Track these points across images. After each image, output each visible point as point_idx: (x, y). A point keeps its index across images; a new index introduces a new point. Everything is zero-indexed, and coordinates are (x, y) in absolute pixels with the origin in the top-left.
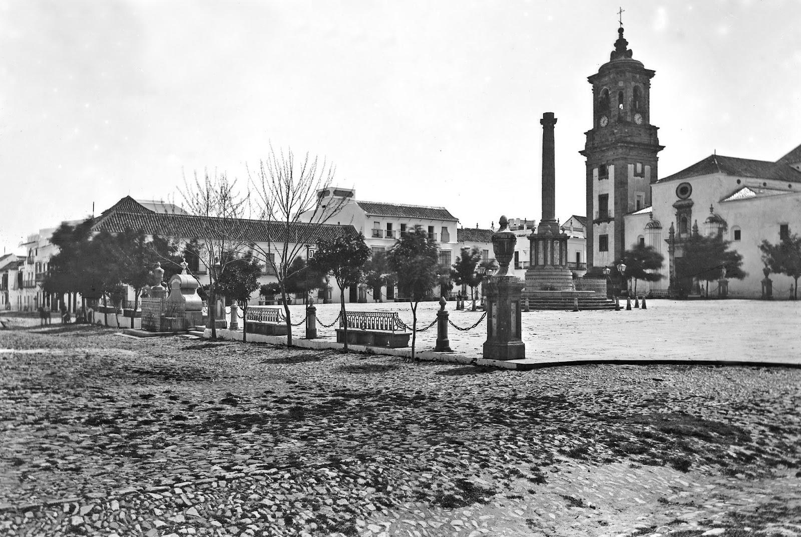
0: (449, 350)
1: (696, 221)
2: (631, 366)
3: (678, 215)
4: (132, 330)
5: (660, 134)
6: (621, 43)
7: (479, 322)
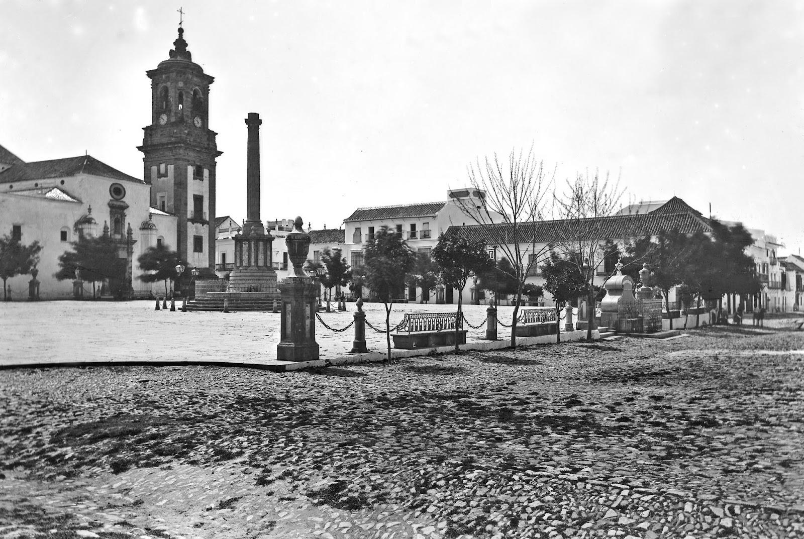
0: (366, 351)
2: (177, 367)
3: (112, 214)
4: (672, 331)
5: (218, 140)
6: (181, 44)
7: (323, 323)
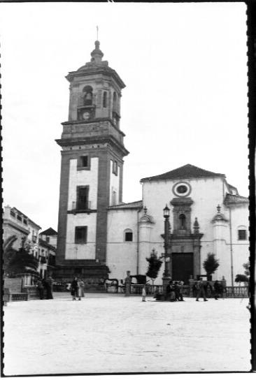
1: (196, 218)
